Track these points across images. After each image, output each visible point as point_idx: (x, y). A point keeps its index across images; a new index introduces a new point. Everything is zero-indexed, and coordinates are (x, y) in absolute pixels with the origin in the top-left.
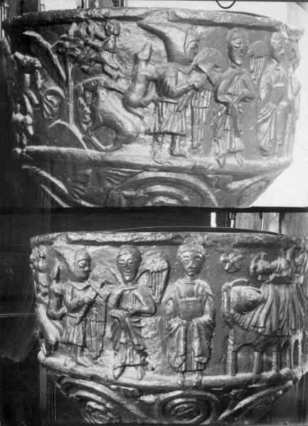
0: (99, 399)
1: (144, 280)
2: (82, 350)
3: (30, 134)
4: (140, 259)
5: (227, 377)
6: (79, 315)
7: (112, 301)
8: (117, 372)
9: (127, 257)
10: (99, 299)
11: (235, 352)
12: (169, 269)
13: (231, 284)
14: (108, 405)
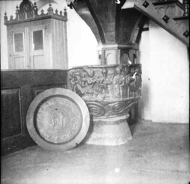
0: (96, 106)
1: (108, 76)
2: (92, 94)
3: (143, 26)
4: (107, 71)
5: (128, 98)
6: (92, 86)
7: (101, 82)
8: (103, 99)
9: (104, 71)
10: (97, 82)
11: (129, 92)
12: (114, 73)
13: (128, 76)
14: (98, 108)
